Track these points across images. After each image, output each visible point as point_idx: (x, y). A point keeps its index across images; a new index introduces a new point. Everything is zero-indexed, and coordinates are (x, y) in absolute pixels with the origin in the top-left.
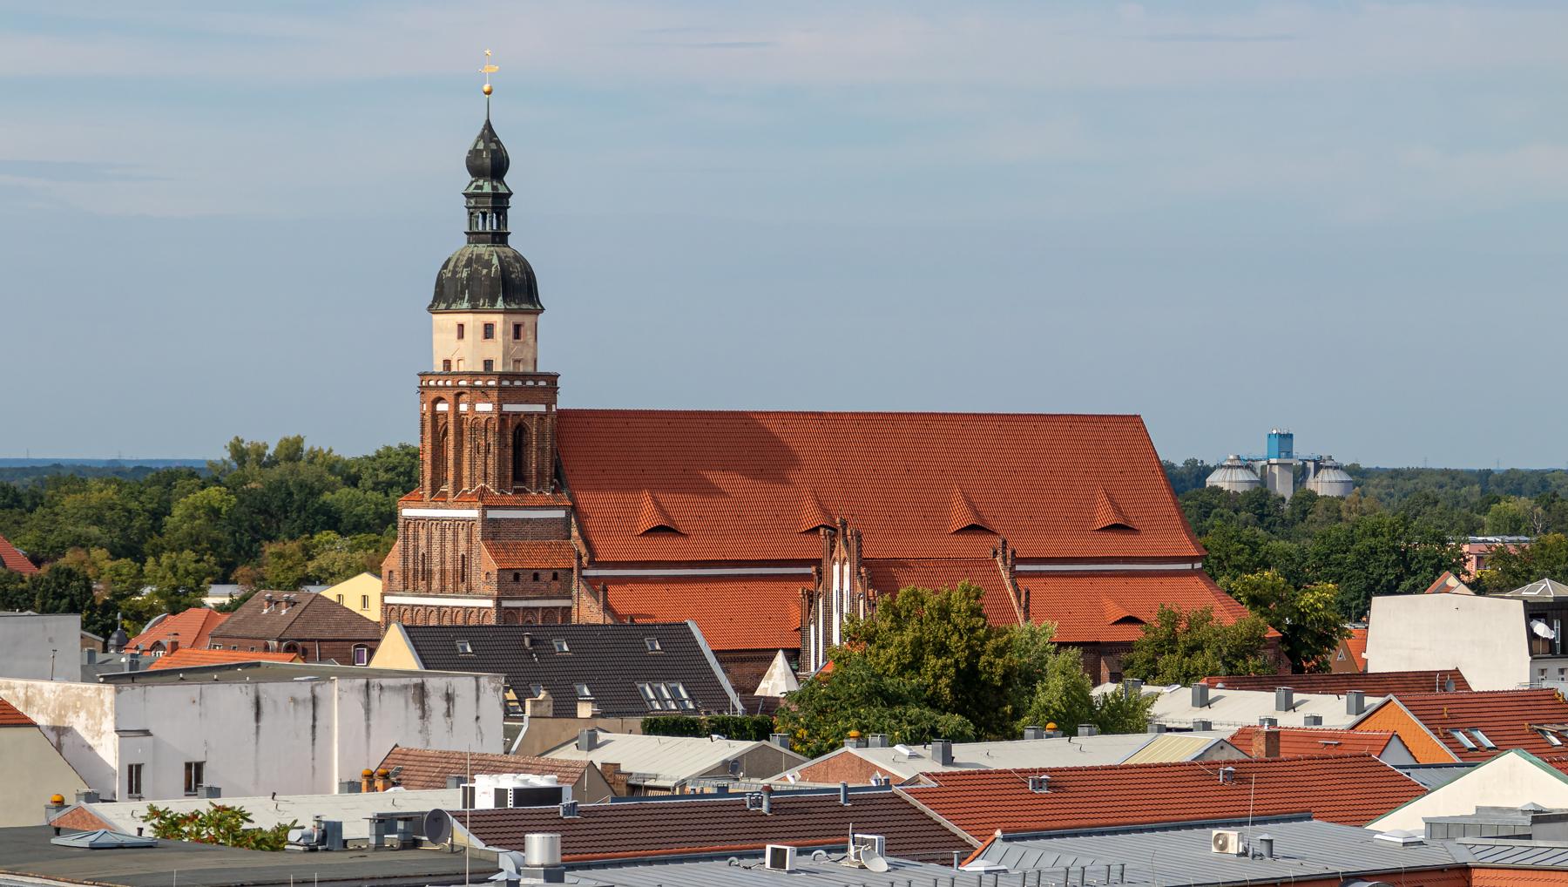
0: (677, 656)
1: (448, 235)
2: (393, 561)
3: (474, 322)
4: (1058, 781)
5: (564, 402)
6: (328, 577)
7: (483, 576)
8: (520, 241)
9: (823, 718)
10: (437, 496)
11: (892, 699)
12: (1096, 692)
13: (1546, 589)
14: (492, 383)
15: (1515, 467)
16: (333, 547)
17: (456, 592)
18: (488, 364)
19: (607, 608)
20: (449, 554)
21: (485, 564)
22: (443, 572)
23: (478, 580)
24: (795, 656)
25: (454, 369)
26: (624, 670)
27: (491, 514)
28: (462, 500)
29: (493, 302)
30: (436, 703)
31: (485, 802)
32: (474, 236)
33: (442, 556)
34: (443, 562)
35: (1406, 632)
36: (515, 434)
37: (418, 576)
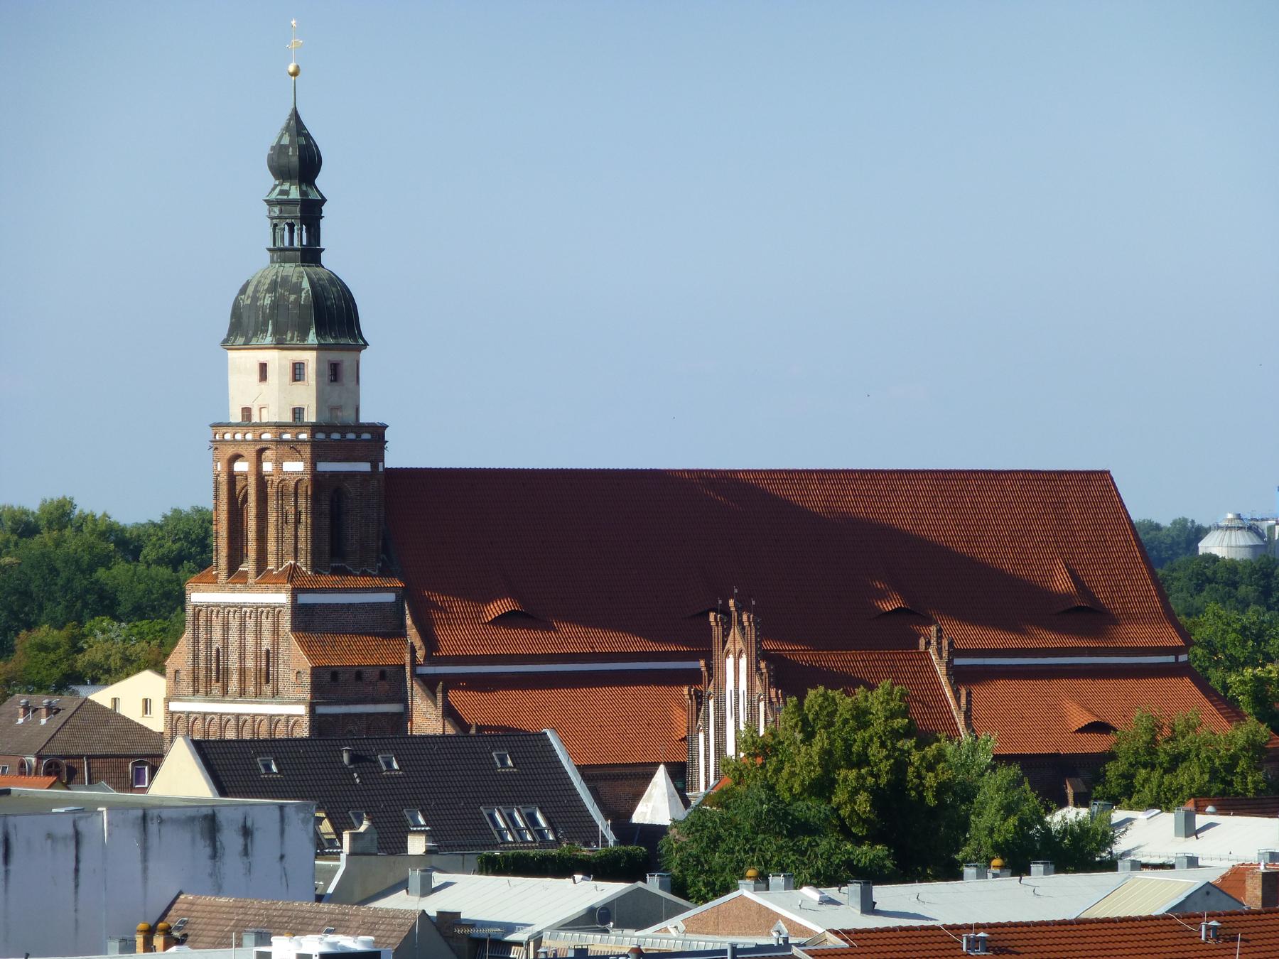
0: (537, 779)
1: (246, 248)
2: (180, 657)
5: (394, 458)
6: (105, 674)
7: (293, 676)
11: (802, 828)
14: (303, 436)
16: (105, 637)
18: (298, 412)
19: (450, 713)
21: (295, 662)
22: (242, 671)
24: (681, 775)
25: (255, 419)
27: (304, 599)
29: (304, 335)
30: (230, 839)
32: (280, 253)
33: (240, 653)
34: (242, 659)
36: (326, 492)
37: (212, 676)
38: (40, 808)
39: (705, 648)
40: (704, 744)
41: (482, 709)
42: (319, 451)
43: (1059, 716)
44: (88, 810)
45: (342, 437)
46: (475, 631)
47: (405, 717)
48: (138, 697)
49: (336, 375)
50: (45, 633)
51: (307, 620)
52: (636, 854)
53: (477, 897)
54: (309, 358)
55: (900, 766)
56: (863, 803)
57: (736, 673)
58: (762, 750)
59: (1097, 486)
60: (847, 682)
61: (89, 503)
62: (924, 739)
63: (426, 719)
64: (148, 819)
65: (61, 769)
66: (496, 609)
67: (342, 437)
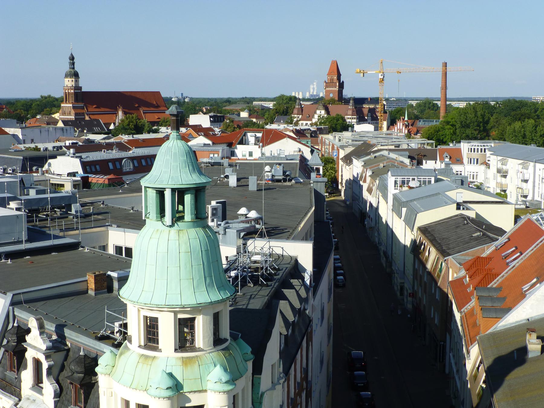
0: (99, 125)
1: (66, 68)
2: (61, 111)
4: (144, 140)
5: (83, 90)
6: (54, 113)
8: (76, 69)
9: (115, 133)
10: (66, 103)
11: (126, 129)
12: (153, 128)
13: (212, 114)
16: (54, 109)
19: (90, 117)
21: (73, 112)
23: (72, 114)
24: (114, 124)
26: (92, 127)
30: (65, 131)
31: (67, 144)
32: (70, 68)
33: (67, 111)
35: (194, 120)
36: (76, 94)
37: (64, 114)
38: (45, 127)
39: (117, 110)
40: (117, 121)
41: (93, 117)
42: (75, 89)
43: (154, 117)
44: (49, 128)
45: (77, 88)
46: (92, 109)
47: (85, 118)
48: (56, 116)
49: (76, 81)
50: (48, 109)
51: (74, 108)
52: (109, 132)
53: (91, 137)
54: (70, 79)
55: (137, 123)
56: (133, 126)
57: (120, 113)
58: (122, 121)
59: (158, 93)
60: (131, 114)
61: (52, 95)
62: (139, 119)
63: (87, 118)
64: (56, 129)
65: (48, 124)
66: (95, 106)
67: (77, 88)
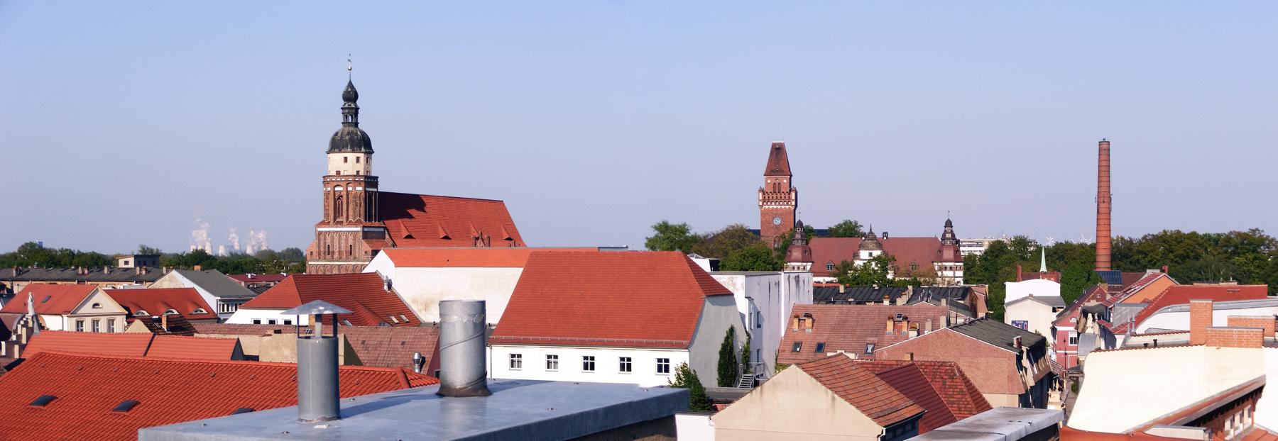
1: (335, 123)
3: (352, 157)
15: (1171, 227)
17: (325, 259)
20: (343, 245)
22: (340, 252)
28: (350, 224)
